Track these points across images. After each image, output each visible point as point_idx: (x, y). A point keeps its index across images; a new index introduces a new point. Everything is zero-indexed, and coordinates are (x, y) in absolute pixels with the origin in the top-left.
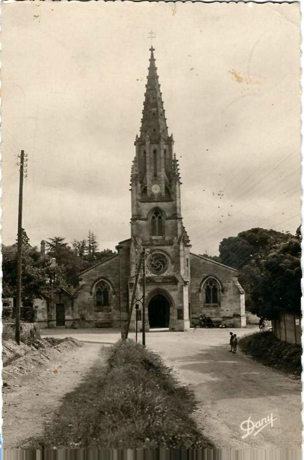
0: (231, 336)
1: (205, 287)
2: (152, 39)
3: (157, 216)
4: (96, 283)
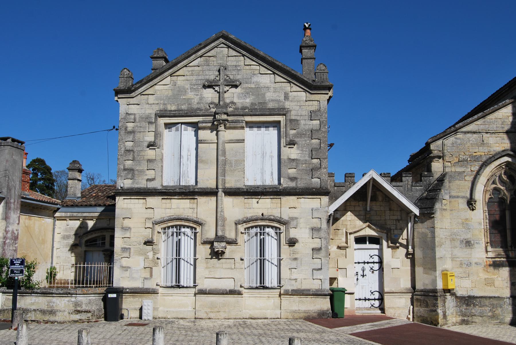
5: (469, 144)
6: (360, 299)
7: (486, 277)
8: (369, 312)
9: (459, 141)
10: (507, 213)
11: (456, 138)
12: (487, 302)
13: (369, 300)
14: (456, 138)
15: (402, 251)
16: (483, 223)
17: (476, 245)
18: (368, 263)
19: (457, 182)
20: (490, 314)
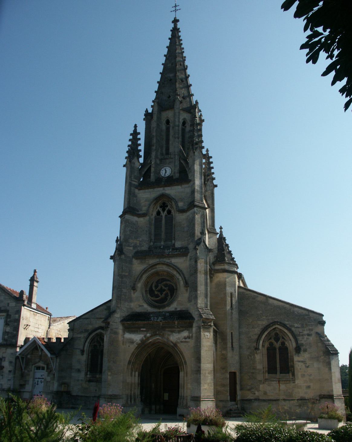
0: (321, 400)
1: (267, 345)
2: (176, 12)
3: (164, 210)
4: (91, 336)
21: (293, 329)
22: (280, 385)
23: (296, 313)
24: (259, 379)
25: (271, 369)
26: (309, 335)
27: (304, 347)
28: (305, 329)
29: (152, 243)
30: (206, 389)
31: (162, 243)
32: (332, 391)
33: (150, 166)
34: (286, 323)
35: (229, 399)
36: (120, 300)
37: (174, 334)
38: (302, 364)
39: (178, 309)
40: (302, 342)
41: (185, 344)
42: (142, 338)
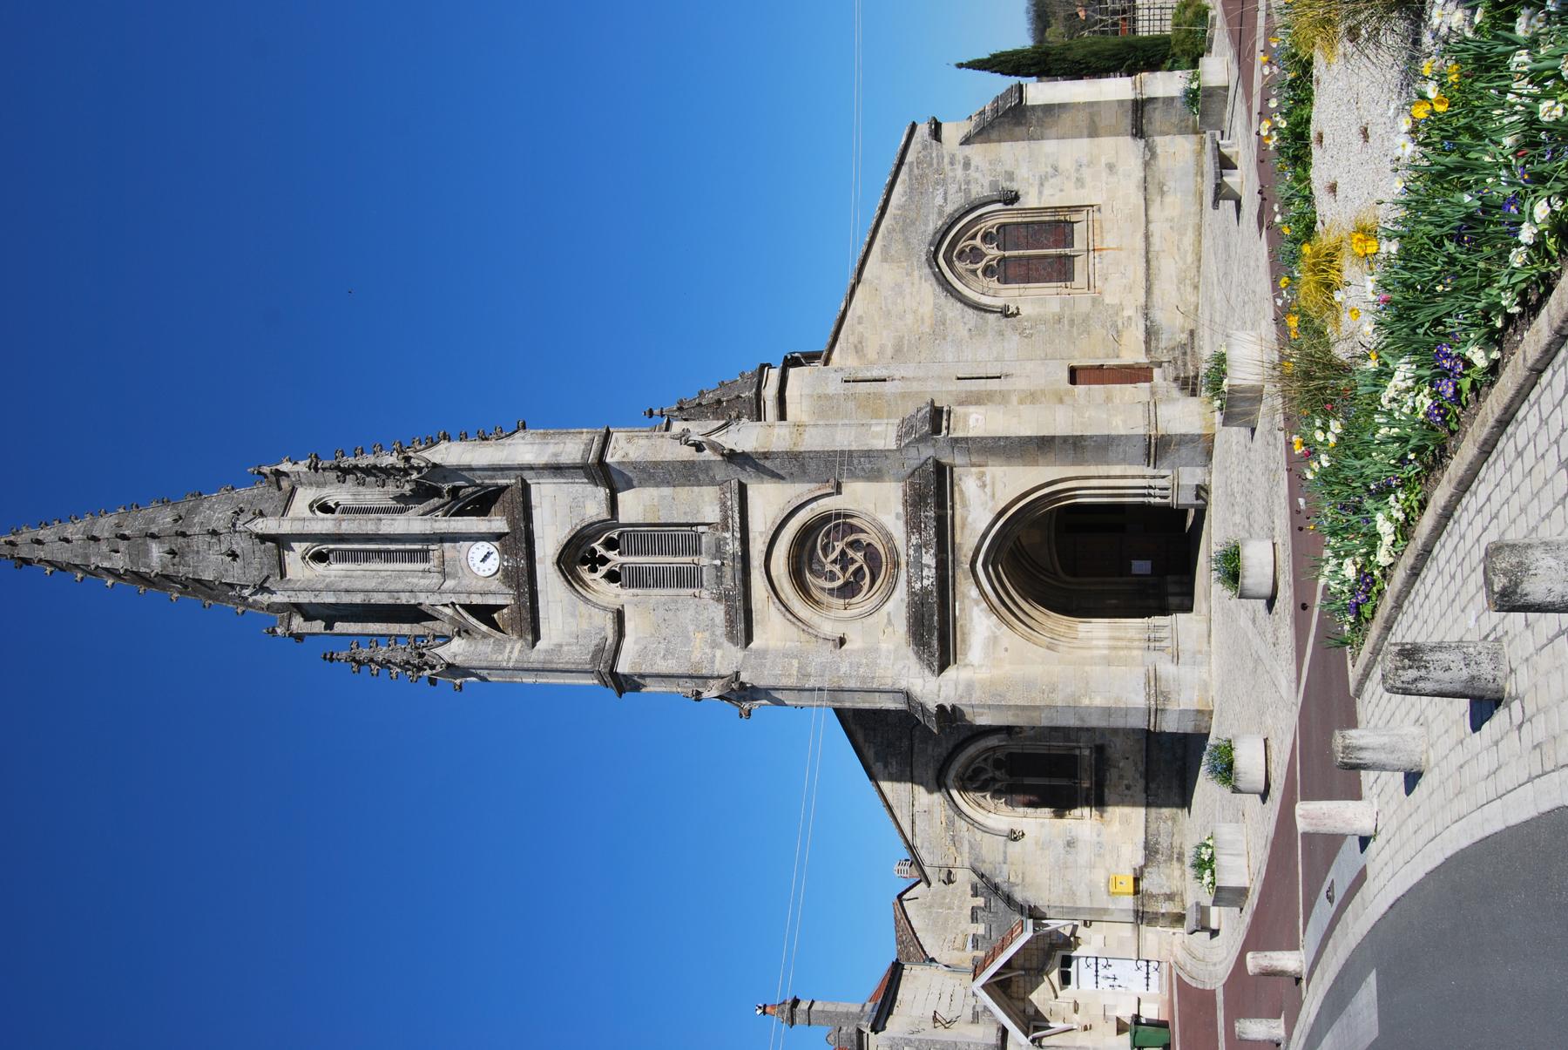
1: (993, 283)
5: (930, 831)
6: (1148, 985)
7: (1117, 823)
8: (1164, 977)
9: (926, 844)
10: (1028, 781)
11: (922, 847)
12: (1153, 826)
13: (1148, 974)
14: (922, 847)
15: (1082, 931)
16: (1042, 820)
17: (1073, 834)
18: (1097, 971)
19: (984, 851)
20: (1170, 823)
21: (949, 209)
22: (1105, 247)
23: (904, 199)
24: (1089, 304)
25: (1062, 270)
26: (967, 165)
27: (1000, 178)
28: (951, 174)
29: (705, 593)
30: (1125, 422)
31: (704, 560)
32: (1121, 103)
33: (466, 607)
34: (931, 228)
35: (1147, 385)
36: (873, 678)
37: (970, 519)
38: (1046, 184)
39: (900, 509)
40: (986, 184)
41: (999, 486)
42: (981, 610)
